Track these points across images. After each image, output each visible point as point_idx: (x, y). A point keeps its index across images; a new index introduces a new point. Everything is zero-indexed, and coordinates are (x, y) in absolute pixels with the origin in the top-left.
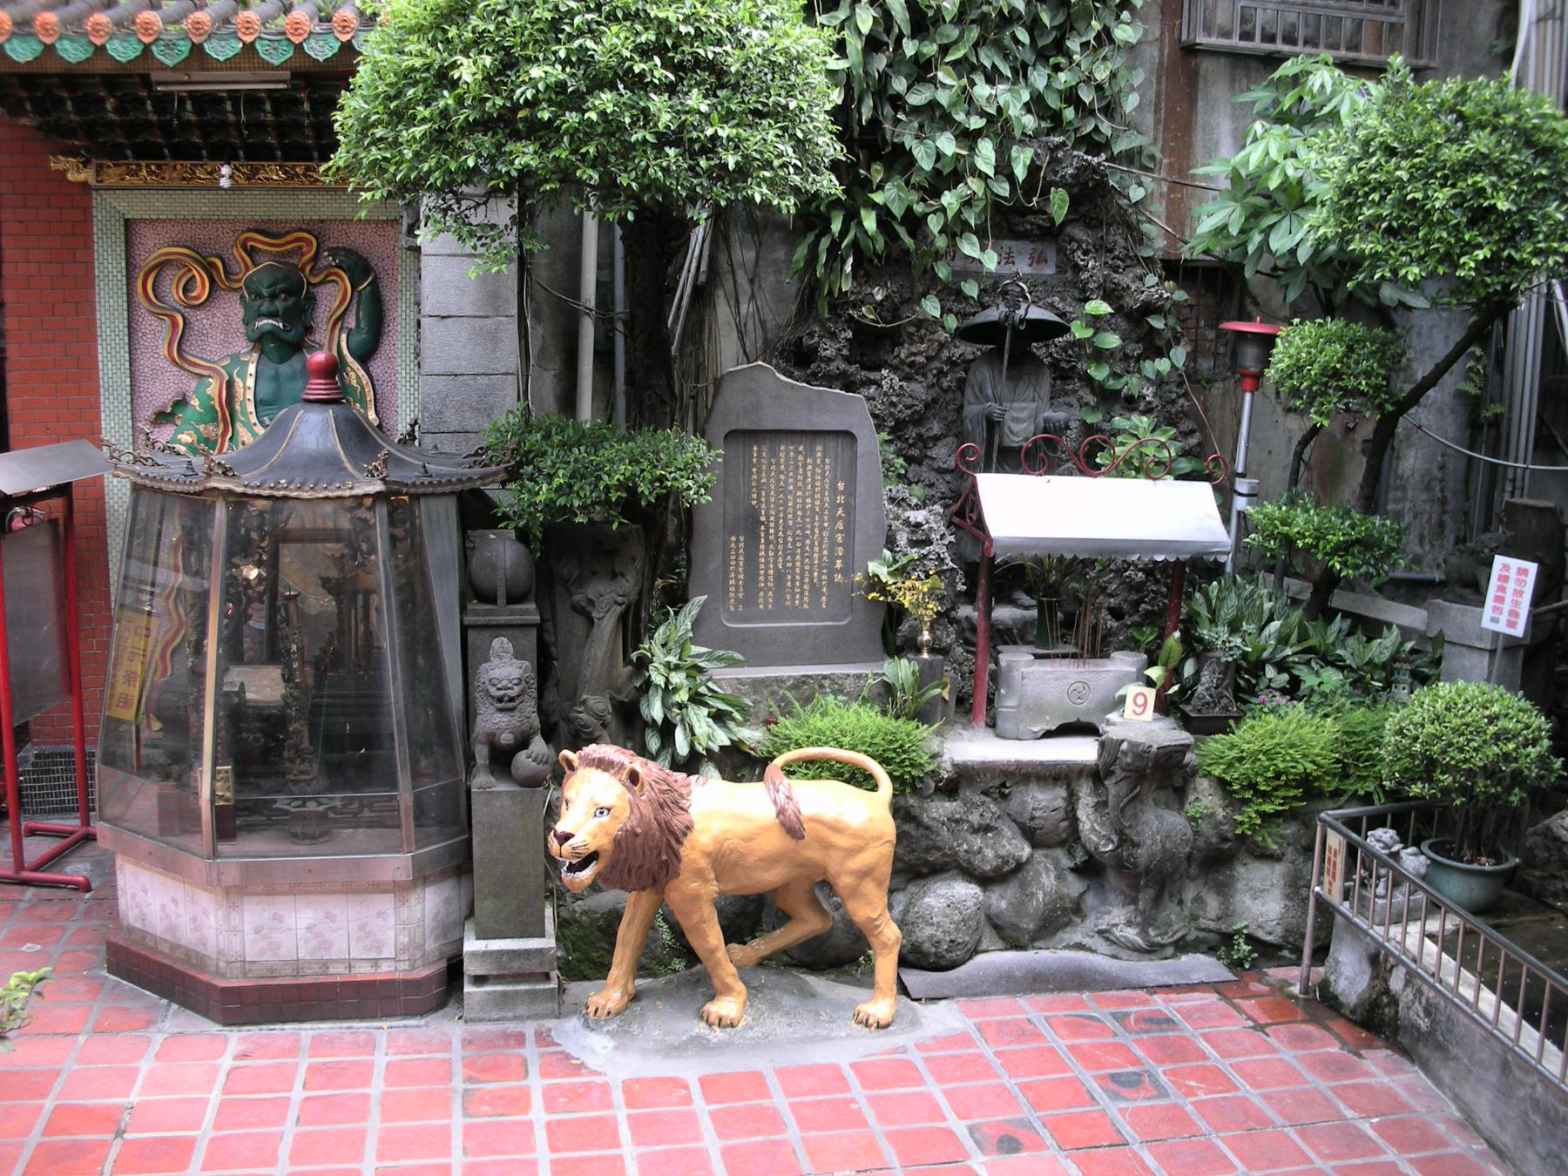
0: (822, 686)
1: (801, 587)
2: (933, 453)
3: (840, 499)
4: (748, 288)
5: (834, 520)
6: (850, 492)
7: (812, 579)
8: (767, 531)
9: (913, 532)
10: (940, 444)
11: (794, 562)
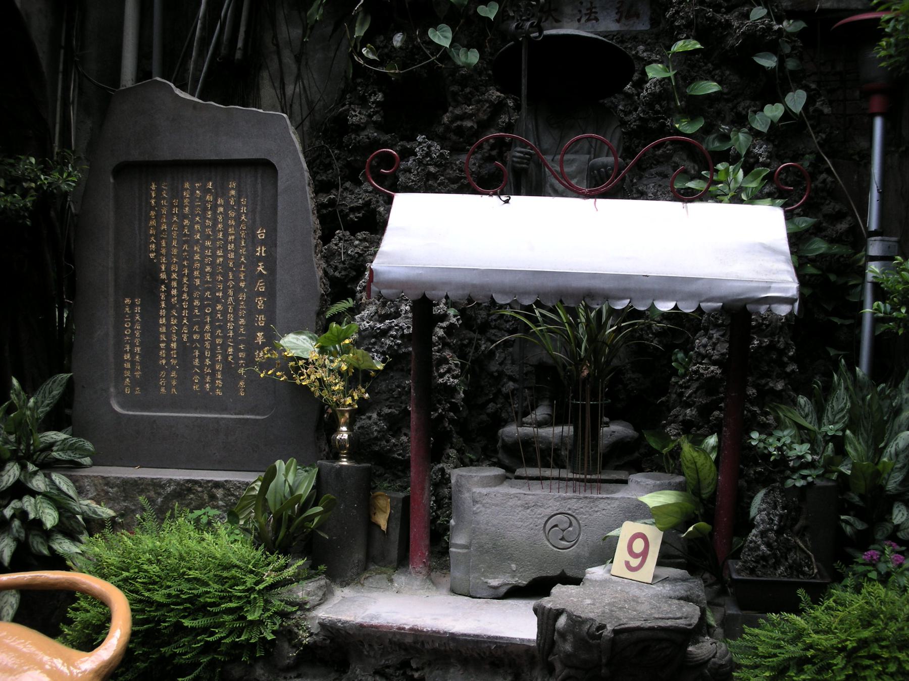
0: (213, 497)
1: (212, 366)
3: (261, 251)
4: (294, 67)
5: (252, 282)
6: (271, 242)
7: (225, 356)
8: (168, 292)
11: (202, 333)
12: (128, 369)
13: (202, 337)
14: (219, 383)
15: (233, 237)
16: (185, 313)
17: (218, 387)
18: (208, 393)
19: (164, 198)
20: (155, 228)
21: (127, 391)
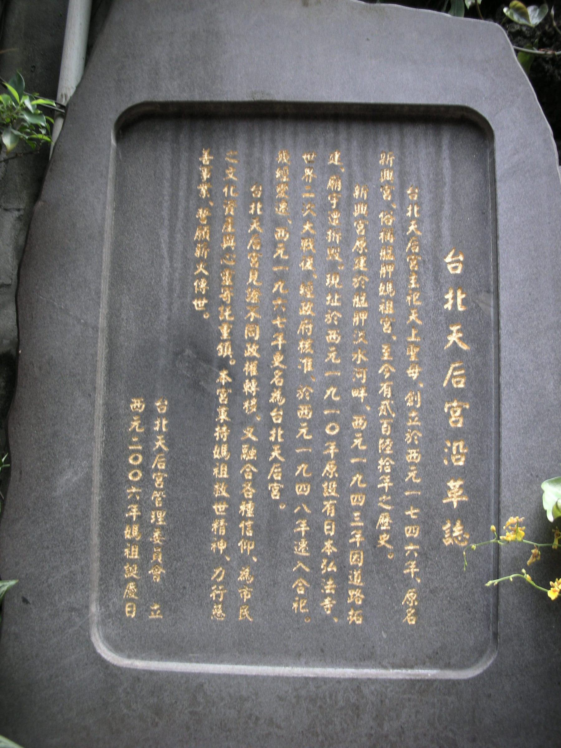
1: (340, 558)
6: (484, 278)
7: (372, 535)
8: (236, 387)
11: (316, 481)
12: (132, 562)
13: (317, 490)
14: (355, 596)
15: (391, 269)
16: (276, 435)
17: (353, 606)
18: (327, 619)
19: (230, 183)
20: (208, 245)
21: (131, 612)
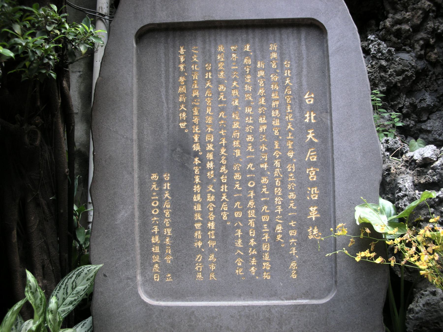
1: (258, 247)
2: (428, 126)
6: (324, 106)
7: (273, 236)
8: (203, 166)
9: (420, 174)
10: (434, 116)
11: (245, 210)
